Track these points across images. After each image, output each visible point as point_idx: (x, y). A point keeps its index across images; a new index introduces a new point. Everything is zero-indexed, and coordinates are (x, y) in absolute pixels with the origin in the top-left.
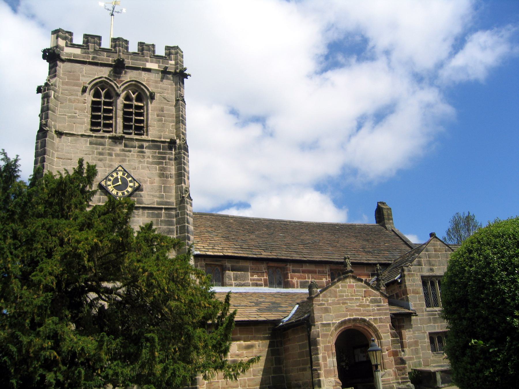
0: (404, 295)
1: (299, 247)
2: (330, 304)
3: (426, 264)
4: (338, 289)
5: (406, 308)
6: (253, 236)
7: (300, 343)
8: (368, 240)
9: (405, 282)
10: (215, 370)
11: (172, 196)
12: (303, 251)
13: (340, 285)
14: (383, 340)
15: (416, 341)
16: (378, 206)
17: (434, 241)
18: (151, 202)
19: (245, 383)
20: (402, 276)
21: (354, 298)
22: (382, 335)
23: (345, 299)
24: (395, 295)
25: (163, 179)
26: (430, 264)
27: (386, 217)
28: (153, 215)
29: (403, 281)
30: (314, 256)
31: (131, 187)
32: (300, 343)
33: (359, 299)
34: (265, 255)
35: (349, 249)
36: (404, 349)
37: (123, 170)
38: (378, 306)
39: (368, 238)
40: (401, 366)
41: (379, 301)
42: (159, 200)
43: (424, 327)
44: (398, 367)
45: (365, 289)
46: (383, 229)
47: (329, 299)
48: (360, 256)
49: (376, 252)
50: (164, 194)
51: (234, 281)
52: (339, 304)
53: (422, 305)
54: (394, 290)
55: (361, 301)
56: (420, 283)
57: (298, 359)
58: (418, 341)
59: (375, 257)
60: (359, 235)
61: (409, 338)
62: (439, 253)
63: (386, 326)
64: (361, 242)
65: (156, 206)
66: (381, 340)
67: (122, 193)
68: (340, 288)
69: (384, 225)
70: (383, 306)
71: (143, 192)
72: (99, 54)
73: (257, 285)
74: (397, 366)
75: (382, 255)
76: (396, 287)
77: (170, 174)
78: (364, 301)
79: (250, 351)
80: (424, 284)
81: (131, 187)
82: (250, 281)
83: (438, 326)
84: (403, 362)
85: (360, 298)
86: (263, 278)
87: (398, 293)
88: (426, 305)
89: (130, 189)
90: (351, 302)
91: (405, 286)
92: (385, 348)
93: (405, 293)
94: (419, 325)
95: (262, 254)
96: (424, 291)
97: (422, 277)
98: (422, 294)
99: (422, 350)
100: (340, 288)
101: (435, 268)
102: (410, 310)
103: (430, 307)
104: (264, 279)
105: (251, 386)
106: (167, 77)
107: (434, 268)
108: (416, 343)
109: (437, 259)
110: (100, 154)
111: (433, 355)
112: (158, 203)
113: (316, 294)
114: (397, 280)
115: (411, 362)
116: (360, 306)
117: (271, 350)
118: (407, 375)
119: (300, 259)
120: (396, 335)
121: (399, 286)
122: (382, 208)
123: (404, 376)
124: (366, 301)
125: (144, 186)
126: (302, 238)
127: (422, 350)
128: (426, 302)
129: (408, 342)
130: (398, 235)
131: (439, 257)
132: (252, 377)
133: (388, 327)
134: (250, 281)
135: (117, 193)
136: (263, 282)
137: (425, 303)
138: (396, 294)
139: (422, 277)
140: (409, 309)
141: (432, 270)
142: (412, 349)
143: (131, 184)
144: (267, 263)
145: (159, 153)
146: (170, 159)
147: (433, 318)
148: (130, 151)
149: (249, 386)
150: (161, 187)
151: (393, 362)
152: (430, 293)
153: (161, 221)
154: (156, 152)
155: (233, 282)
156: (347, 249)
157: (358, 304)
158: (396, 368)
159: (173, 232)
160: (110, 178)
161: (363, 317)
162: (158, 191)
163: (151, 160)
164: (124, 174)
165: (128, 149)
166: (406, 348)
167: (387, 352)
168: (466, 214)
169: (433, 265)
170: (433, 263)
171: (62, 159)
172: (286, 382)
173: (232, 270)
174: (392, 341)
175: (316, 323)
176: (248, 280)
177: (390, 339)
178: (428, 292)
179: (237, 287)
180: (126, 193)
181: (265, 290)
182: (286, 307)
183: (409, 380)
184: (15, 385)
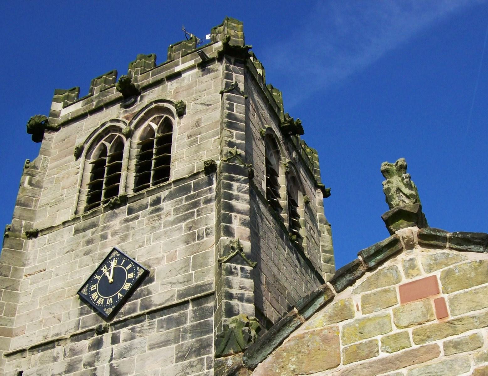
4: (341, 325)
10: (248, 369)
11: (209, 270)
18: (168, 297)
21: (440, 343)
25: (193, 243)
28: (170, 323)
31: (129, 281)
37: (87, 286)
42: (182, 288)
50: (193, 272)
65: (176, 301)
67: (127, 282)
71: (153, 283)
72: (106, 94)
77: (207, 229)
81: (129, 281)
89: (127, 286)
100: (358, 315)
106: (209, 69)
110: (89, 242)
112: (180, 296)
125: (156, 270)
135: (105, 300)
143: (131, 276)
145: (187, 199)
146: (207, 201)
148: (137, 218)
150: (187, 260)
153: (185, 330)
154: (182, 199)
159: (209, 345)
160: (97, 277)
162: (181, 272)
163: (171, 218)
164: (119, 263)
165: (133, 215)
171: (31, 274)
180: (120, 295)
184: (255, 95)
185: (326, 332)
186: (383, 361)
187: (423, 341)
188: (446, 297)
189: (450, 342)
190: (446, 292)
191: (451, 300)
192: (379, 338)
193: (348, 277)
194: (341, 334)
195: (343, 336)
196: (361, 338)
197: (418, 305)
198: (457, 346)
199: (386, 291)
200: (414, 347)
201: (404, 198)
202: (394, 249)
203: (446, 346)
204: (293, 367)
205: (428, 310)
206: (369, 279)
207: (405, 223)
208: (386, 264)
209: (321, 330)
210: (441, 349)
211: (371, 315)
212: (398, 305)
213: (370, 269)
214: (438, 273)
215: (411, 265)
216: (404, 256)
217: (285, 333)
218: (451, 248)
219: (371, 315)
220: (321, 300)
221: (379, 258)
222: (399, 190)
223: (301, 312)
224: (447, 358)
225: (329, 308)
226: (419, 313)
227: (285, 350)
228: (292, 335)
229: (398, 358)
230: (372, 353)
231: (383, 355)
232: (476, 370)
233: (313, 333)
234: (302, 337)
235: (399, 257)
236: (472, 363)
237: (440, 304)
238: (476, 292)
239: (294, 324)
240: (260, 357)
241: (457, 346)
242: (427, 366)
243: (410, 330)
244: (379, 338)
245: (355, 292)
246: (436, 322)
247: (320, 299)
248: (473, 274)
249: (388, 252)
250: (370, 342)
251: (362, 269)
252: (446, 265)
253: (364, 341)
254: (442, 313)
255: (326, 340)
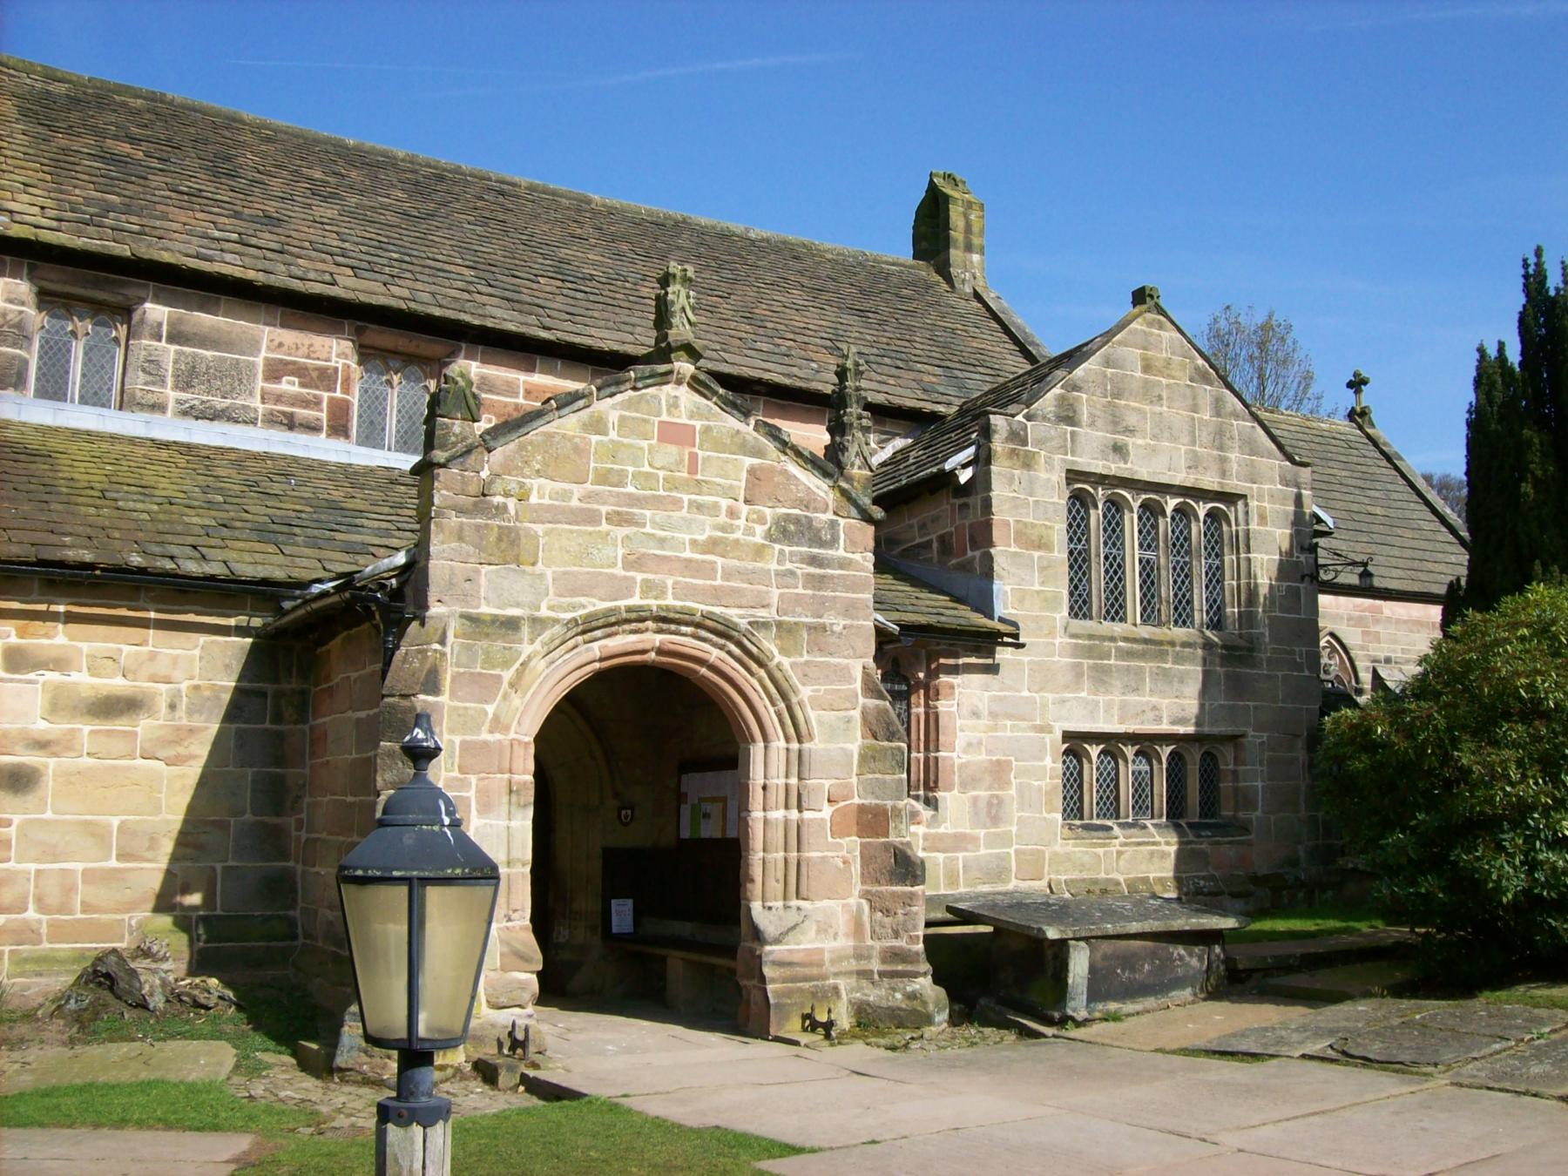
0: (975, 546)
1: (535, 286)
2: (540, 515)
3: (1099, 423)
4: (595, 438)
5: (976, 610)
6: (329, 211)
7: (362, 714)
8: (861, 313)
9: (988, 488)
12: (548, 304)
13: (613, 417)
14: (814, 746)
15: (998, 762)
16: (933, 191)
17: (1150, 324)
19: (70, 890)
20: (982, 461)
21: (686, 498)
22: (813, 717)
23: (633, 500)
24: (935, 545)
26: (1115, 423)
27: (957, 234)
29: (982, 482)
30: (593, 331)
32: (362, 714)
33: (713, 509)
34: (347, 286)
35: (770, 333)
36: (939, 794)
38: (813, 560)
39: (866, 305)
40: (894, 888)
41: (826, 535)
43: (1044, 706)
44: (879, 895)
45: (756, 461)
46: (937, 284)
47: (535, 483)
48: (814, 365)
49: (887, 360)
51: (176, 387)
52: (591, 518)
53: (1051, 602)
54: (935, 520)
55: (723, 519)
56: (1056, 499)
57: (350, 799)
58: (1010, 763)
59: (879, 378)
60: (830, 285)
61: (970, 745)
62: (1164, 381)
63: (843, 674)
64: (831, 313)
66: (806, 746)
68: (613, 435)
69: (944, 270)
70: (843, 564)
73: (291, 424)
74: (875, 888)
75: (912, 375)
76: (945, 506)
78: (741, 522)
79: (120, 725)
80: (1079, 501)
82: (256, 403)
83: (1109, 706)
84: (906, 868)
85: (716, 506)
86: (326, 395)
87: (950, 534)
88: (1071, 608)
90: (660, 515)
91: (987, 505)
92: (821, 784)
93: (982, 535)
94: (1026, 693)
95: (334, 283)
96: (1071, 540)
97: (1073, 475)
98: (1060, 554)
99: (1021, 808)
100: (613, 435)
101: (1133, 443)
102: (991, 617)
103: (1087, 616)
104: (331, 400)
105: (105, 912)
107: (1130, 441)
108: (999, 772)
109: (1147, 408)
111: (1066, 830)
113: (460, 448)
114: (952, 475)
115: (960, 855)
116: (713, 546)
117: (239, 733)
118: (913, 939)
119: (523, 329)
120: (889, 724)
121: (958, 502)
122: (946, 198)
123: (901, 943)
124: (751, 527)
126: (563, 253)
127: (1021, 808)
128: (1071, 594)
129: (961, 766)
130: (995, 317)
131: (1160, 398)
132: (113, 863)
133: (851, 680)
134: (256, 403)
136: (324, 416)
137: (1065, 593)
138: (942, 539)
139: (1073, 475)
140: (988, 612)
141: (1119, 450)
142: (975, 800)
144: (359, 332)
147: (1095, 668)
149: (86, 907)
151: (856, 868)
152: (1098, 555)
155: (171, 395)
156: (761, 331)
157: (701, 538)
158: (866, 895)
161: (717, 610)
166: (949, 788)
167: (827, 811)
168: (1260, 319)
169: (1130, 431)
170: (1132, 420)
172: (300, 904)
173: (172, 339)
174: (864, 748)
175: (435, 610)
176: (251, 394)
177: (855, 743)
178: (1087, 551)
179: (190, 422)
181: (327, 450)
182: (379, 533)
183: (925, 967)
185: (577, 440)
186: (630, 495)
187: (670, 490)
188: (700, 453)
189: (695, 501)
190: (701, 448)
191: (703, 459)
192: (631, 469)
193: (613, 389)
194: (592, 450)
195: (596, 453)
196: (613, 463)
197: (673, 449)
198: (699, 507)
199: (644, 421)
200: (662, 492)
201: (685, 321)
202: (664, 379)
203: (691, 503)
204: (537, 467)
205: (682, 461)
206: (630, 399)
207: (686, 357)
208: (650, 390)
209: (574, 437)
210: (686, 504)
211: (626, 441)
212: (654, 442)
213: (635, 389)
214: (698, 424)
215: (674, 404)
216: (669, 389)
217: (535, 424)
218: (716, 404)
219: (626, 441)
220: (581, 403)
221: (649, 381)
222: (683, 310)
223: (558, 408)
224: (688, 516)
225: (584, 414)
226: (672, 460)
227: (531, 443)
228: (540, 429)
229: (645, 498)
230: (621, 483)
231: (630, 489)
232: (710, 537)
233: (564, 436)
234: (550, 436)
235: (667, 388)
236: (708, 528)
237: (694, 457)
238: (727, 461)
239: (547, 418)
240: (502, 440)
241: (699, 507)
242: (669, 517)
243: (661, 474)
244: (631, 469)
245: (614, 407)
246: (685, 475)
247: (1071, 975)
248: (729, 441)
249: (658, 380)
250: (622, 470)
251: (628, 385)
252: (707, 419)
253: (616, 467)
254: (693, 469)
255: (577, 450)
